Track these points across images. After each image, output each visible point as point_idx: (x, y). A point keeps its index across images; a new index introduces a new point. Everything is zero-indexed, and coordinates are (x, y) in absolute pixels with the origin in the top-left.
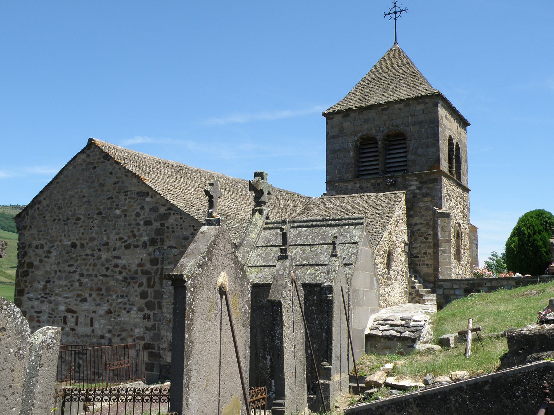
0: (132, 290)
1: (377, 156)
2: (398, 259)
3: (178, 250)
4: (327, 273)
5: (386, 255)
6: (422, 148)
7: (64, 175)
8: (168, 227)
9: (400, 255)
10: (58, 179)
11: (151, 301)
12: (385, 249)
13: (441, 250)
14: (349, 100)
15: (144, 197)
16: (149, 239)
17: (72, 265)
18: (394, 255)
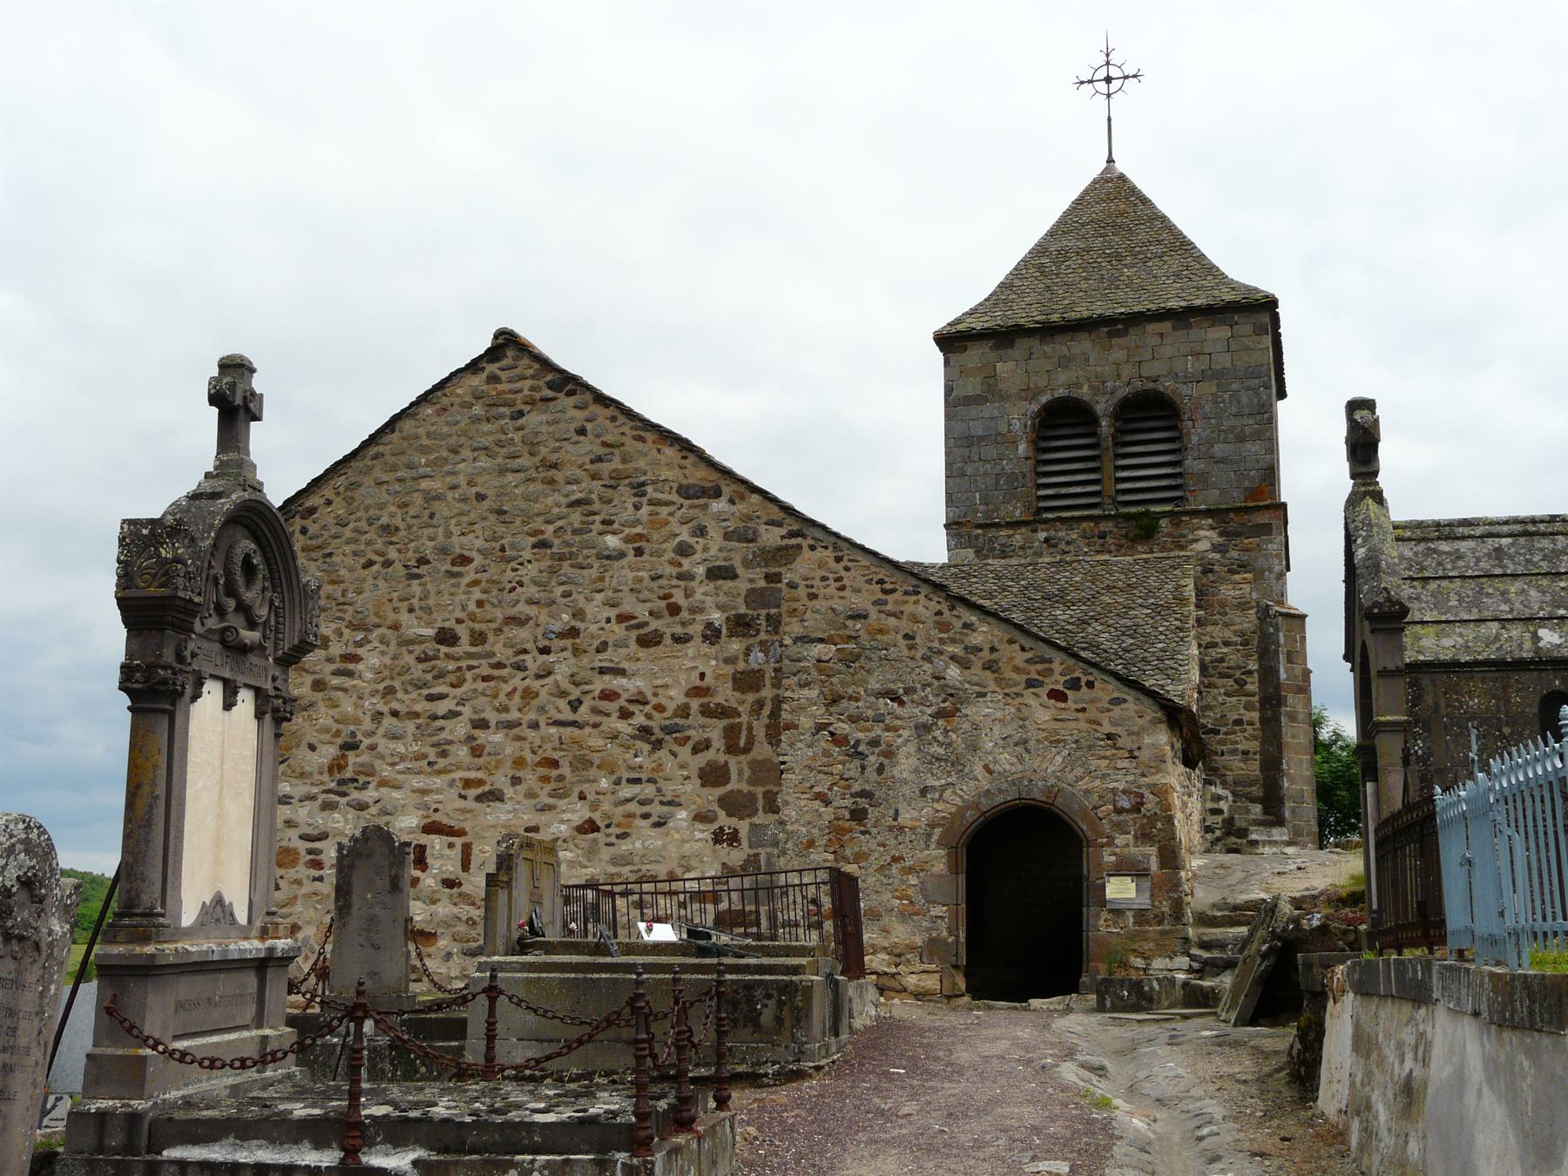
0: (670, 764)
3: (833, 648)
6: (1225, 441)
7: (401, 431)
8: (792, 586)
10: (377, 444)
11: (740, 791)
13: (1287, 713)
14: (1005, 302)
15: (702, 501)
16: (728, 618)
17: (442, 697)
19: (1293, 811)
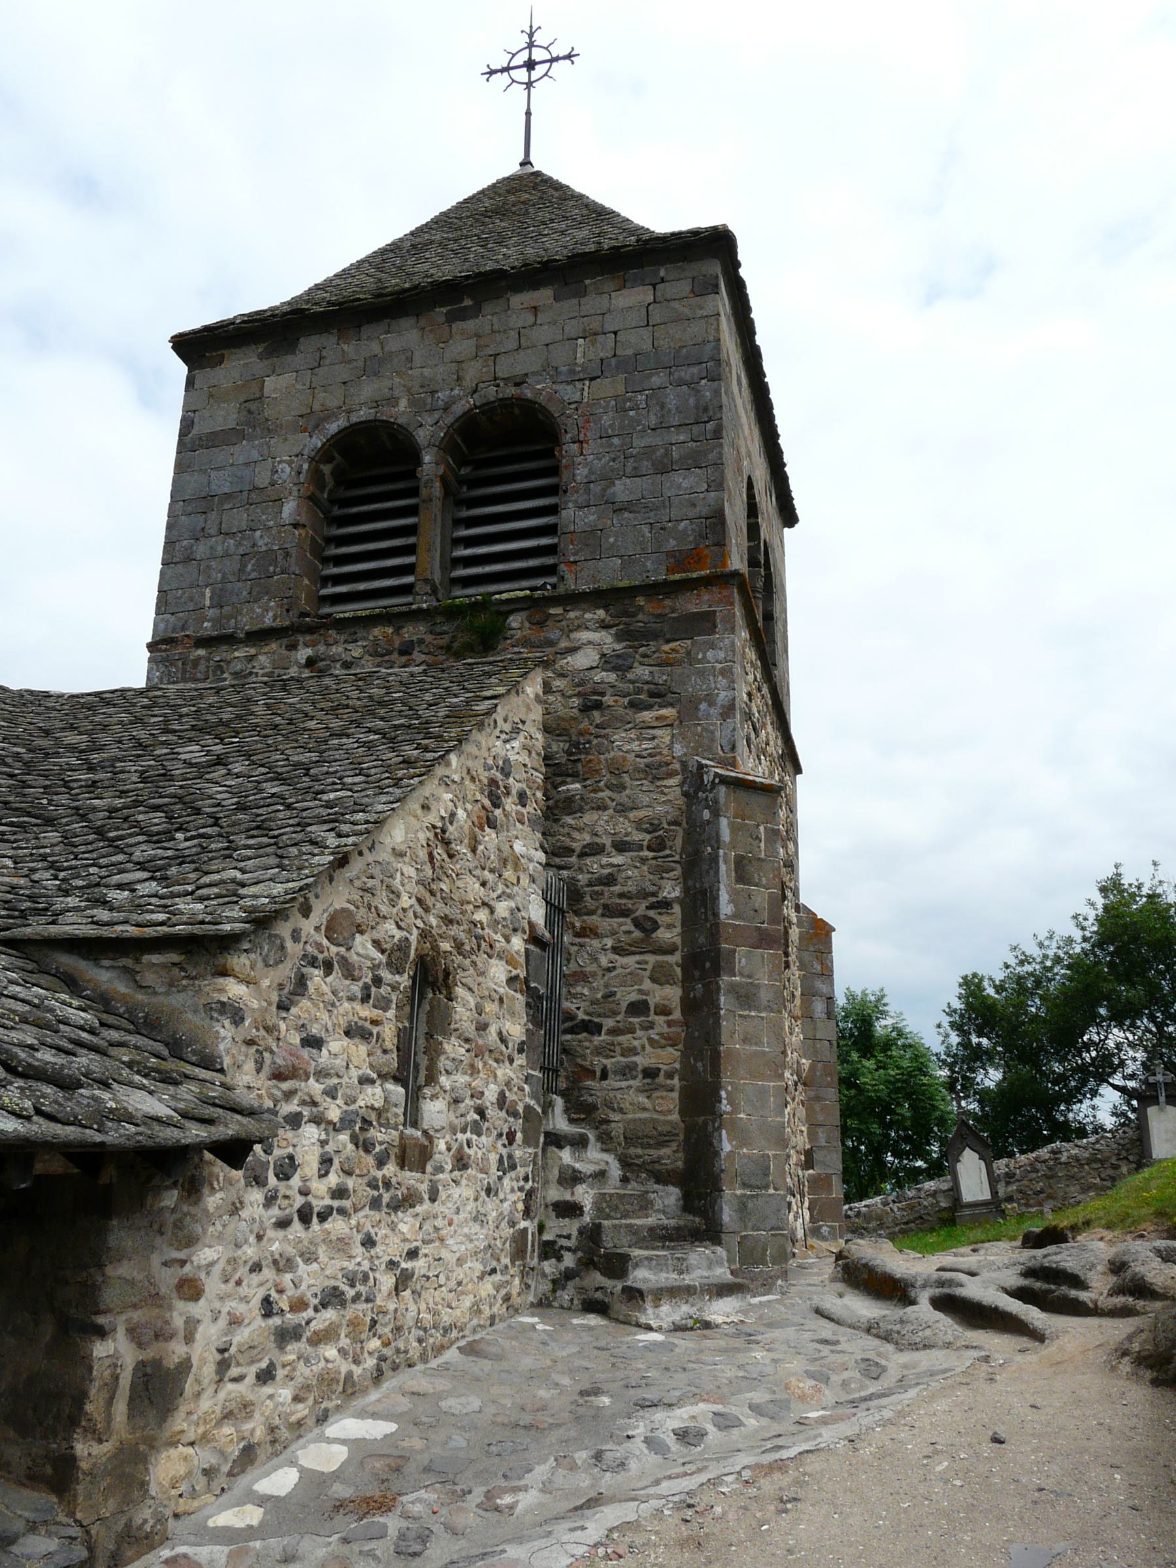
1: (411, 530)
2: (482, 1027)
4: (431, 1133)
5: (404, 980)
9: (501, 1000)
12: (398, 934)
13: (734, 989)
18: (460, 991)
19: (742, 1207)
